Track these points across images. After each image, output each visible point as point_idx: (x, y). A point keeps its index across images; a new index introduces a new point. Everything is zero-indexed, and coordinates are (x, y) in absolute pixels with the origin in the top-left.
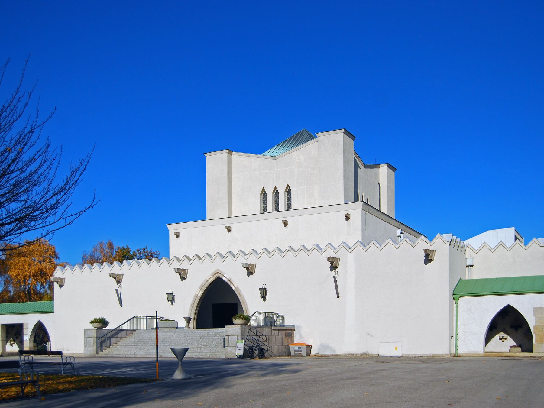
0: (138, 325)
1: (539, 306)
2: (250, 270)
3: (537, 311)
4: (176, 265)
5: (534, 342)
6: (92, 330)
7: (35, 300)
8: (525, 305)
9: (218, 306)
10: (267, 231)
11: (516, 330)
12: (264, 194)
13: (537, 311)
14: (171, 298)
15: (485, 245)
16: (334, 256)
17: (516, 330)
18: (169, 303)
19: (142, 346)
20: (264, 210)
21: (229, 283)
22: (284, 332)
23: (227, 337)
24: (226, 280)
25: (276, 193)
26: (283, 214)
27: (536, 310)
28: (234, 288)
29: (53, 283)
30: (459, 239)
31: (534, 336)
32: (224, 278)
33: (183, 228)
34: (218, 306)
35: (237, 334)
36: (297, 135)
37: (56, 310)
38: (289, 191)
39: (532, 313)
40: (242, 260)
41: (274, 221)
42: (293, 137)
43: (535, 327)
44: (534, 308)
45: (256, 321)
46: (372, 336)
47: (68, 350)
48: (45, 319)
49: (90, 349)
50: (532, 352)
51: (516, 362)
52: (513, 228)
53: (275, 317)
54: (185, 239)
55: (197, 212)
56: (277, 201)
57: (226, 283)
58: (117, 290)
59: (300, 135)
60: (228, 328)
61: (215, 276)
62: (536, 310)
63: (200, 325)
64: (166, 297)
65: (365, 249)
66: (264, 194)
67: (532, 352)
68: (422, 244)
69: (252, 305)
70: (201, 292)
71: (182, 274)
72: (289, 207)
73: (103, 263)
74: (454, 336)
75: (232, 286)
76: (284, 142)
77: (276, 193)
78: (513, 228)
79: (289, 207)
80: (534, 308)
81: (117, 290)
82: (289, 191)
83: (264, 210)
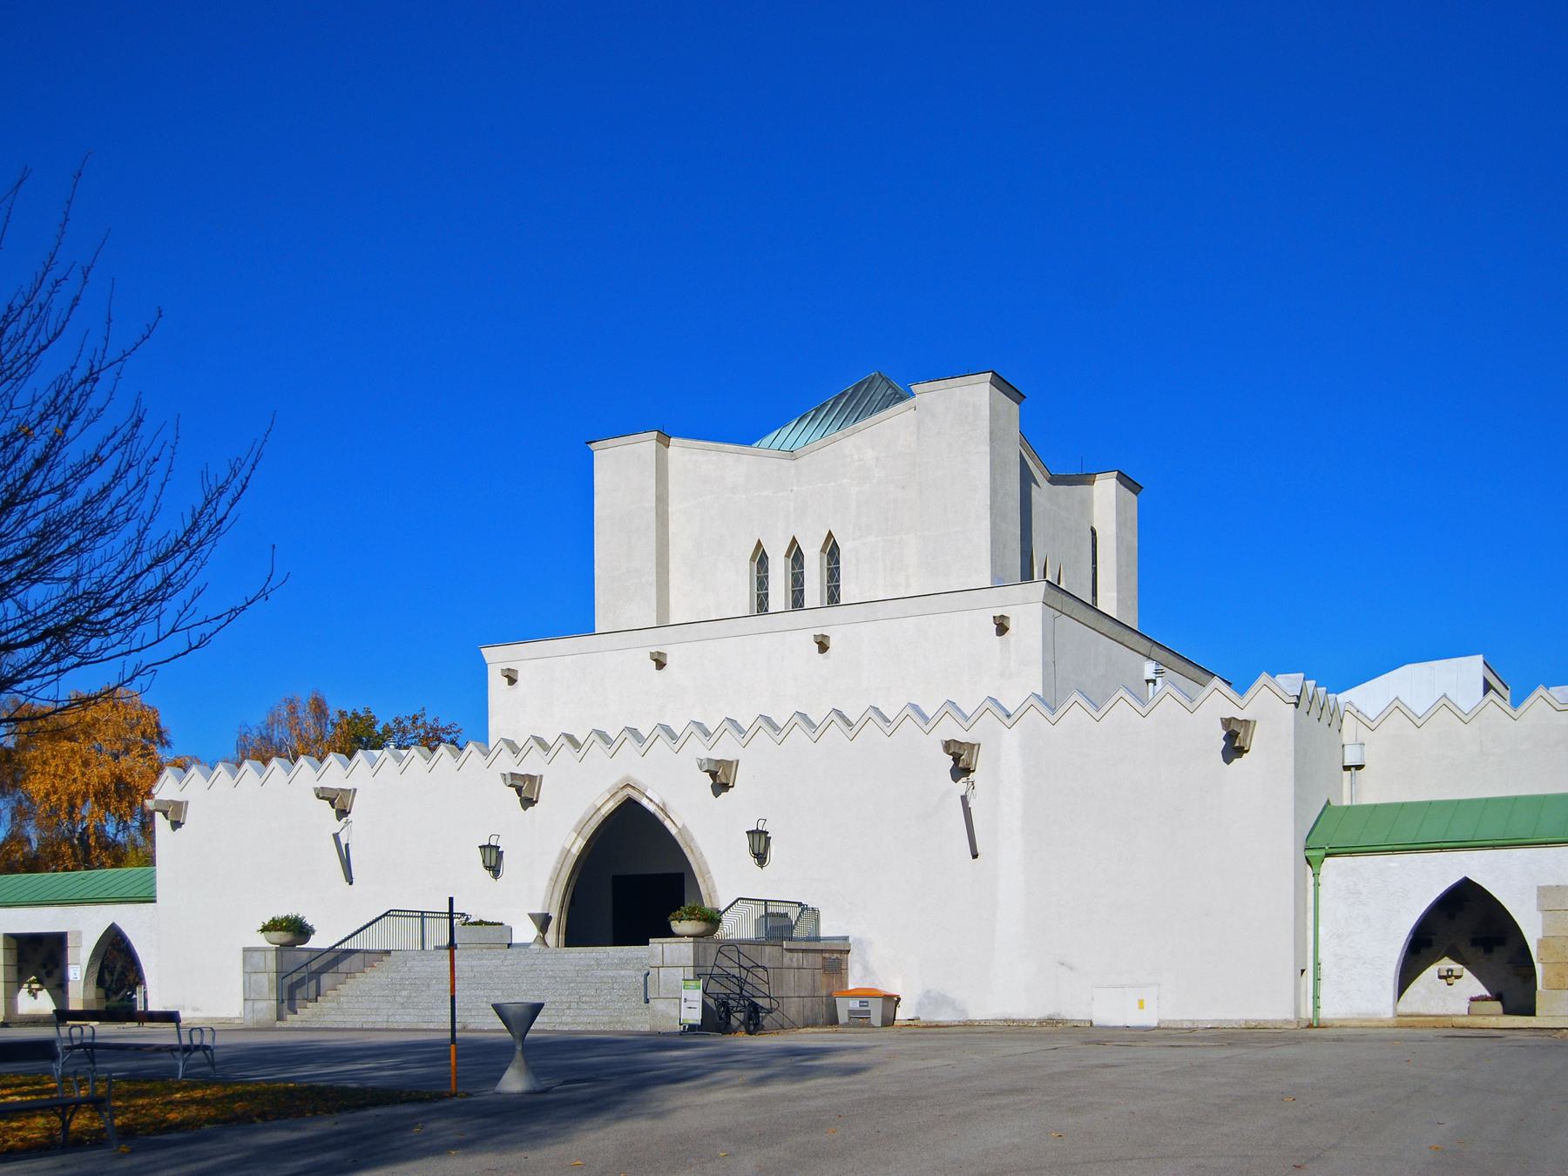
0: (398, 936)
1: (1553, 883)
2: (720, 779)
3: (1548, 896)
4: (507, 763)
5: (1539, 987)
6: (264, 950)
7: (102, 865)
8: (1512, 880)
9: (629, 881)
10: (769, 667)
11: (1489, 950)
12: (761, 559)
13: (1548, 896)
14: (493, 860)
15: (1397, 706)
16: (962, 737)
17: (1489, 950)
18: (488, 874)
19: (409, 997)
20: (762, 605)
21: (660, 815)
22: (818, 958)
23: (653, 972)
24: (651, 808)
25: (796, 555)
26: (816, 618)
27: (1544, 892)
28: (673, 831)
29: (152, 814)
30: (1322, 690)
31: (1538, 967)
32: (645, 802)
33: (528, 657)
34: (629, 881)
35: (684, 962)
36: (856, 389)
37: (160, 893)
38: (832, 551)
39: (1532, 901)
40: (699, 749)
41: (789, 636)
42: (844, 394)
43: (1542, 943)
44: (1539, 888)
45: (738, 926)
46: (1071, 968)
47: (196, 1009)
48: (129, 919)
49: (261, 1005)
50: (1533, 1014)
51: (1487, 1043)
52: (1480, 658)
53: (793, 914)
54: (535, 688)
55: (568, 610)
56: (800, 578)
57: (652, 816)
58: (336, 836)
59: (866, 390)
60: (656, 945)
61: (621, 797)
62: (1544, 892)
63: (576, 936)
64: (478, 856)
65: (1053, 719)
66: (761, 559)
67: (1533, 1014)
68: (1218, 702)
69: (726, 878)
70: (581, 843)
71: (526, 791)
72: (833, 597)
73: (296, 758)
74: (1309, 969)
75: (668, 824)
76: (818, 411)
77: (796, 555)
78: (1480, 658)
79: (833, 597)
80: (1539, 888)
81: (336, 836)
82: (832, 551)
83: (762, 605)
